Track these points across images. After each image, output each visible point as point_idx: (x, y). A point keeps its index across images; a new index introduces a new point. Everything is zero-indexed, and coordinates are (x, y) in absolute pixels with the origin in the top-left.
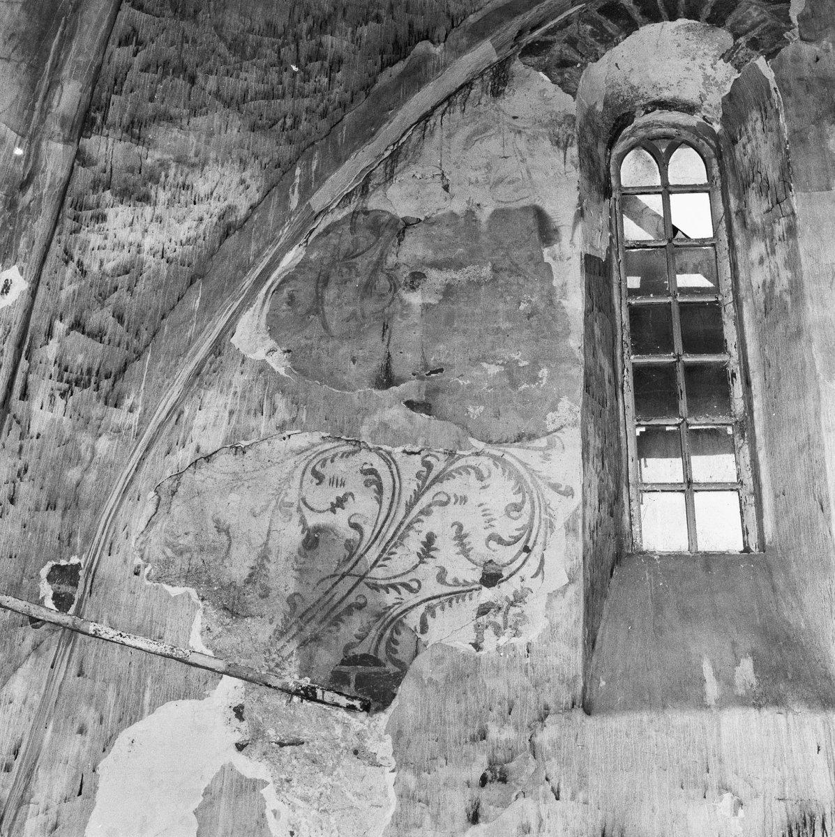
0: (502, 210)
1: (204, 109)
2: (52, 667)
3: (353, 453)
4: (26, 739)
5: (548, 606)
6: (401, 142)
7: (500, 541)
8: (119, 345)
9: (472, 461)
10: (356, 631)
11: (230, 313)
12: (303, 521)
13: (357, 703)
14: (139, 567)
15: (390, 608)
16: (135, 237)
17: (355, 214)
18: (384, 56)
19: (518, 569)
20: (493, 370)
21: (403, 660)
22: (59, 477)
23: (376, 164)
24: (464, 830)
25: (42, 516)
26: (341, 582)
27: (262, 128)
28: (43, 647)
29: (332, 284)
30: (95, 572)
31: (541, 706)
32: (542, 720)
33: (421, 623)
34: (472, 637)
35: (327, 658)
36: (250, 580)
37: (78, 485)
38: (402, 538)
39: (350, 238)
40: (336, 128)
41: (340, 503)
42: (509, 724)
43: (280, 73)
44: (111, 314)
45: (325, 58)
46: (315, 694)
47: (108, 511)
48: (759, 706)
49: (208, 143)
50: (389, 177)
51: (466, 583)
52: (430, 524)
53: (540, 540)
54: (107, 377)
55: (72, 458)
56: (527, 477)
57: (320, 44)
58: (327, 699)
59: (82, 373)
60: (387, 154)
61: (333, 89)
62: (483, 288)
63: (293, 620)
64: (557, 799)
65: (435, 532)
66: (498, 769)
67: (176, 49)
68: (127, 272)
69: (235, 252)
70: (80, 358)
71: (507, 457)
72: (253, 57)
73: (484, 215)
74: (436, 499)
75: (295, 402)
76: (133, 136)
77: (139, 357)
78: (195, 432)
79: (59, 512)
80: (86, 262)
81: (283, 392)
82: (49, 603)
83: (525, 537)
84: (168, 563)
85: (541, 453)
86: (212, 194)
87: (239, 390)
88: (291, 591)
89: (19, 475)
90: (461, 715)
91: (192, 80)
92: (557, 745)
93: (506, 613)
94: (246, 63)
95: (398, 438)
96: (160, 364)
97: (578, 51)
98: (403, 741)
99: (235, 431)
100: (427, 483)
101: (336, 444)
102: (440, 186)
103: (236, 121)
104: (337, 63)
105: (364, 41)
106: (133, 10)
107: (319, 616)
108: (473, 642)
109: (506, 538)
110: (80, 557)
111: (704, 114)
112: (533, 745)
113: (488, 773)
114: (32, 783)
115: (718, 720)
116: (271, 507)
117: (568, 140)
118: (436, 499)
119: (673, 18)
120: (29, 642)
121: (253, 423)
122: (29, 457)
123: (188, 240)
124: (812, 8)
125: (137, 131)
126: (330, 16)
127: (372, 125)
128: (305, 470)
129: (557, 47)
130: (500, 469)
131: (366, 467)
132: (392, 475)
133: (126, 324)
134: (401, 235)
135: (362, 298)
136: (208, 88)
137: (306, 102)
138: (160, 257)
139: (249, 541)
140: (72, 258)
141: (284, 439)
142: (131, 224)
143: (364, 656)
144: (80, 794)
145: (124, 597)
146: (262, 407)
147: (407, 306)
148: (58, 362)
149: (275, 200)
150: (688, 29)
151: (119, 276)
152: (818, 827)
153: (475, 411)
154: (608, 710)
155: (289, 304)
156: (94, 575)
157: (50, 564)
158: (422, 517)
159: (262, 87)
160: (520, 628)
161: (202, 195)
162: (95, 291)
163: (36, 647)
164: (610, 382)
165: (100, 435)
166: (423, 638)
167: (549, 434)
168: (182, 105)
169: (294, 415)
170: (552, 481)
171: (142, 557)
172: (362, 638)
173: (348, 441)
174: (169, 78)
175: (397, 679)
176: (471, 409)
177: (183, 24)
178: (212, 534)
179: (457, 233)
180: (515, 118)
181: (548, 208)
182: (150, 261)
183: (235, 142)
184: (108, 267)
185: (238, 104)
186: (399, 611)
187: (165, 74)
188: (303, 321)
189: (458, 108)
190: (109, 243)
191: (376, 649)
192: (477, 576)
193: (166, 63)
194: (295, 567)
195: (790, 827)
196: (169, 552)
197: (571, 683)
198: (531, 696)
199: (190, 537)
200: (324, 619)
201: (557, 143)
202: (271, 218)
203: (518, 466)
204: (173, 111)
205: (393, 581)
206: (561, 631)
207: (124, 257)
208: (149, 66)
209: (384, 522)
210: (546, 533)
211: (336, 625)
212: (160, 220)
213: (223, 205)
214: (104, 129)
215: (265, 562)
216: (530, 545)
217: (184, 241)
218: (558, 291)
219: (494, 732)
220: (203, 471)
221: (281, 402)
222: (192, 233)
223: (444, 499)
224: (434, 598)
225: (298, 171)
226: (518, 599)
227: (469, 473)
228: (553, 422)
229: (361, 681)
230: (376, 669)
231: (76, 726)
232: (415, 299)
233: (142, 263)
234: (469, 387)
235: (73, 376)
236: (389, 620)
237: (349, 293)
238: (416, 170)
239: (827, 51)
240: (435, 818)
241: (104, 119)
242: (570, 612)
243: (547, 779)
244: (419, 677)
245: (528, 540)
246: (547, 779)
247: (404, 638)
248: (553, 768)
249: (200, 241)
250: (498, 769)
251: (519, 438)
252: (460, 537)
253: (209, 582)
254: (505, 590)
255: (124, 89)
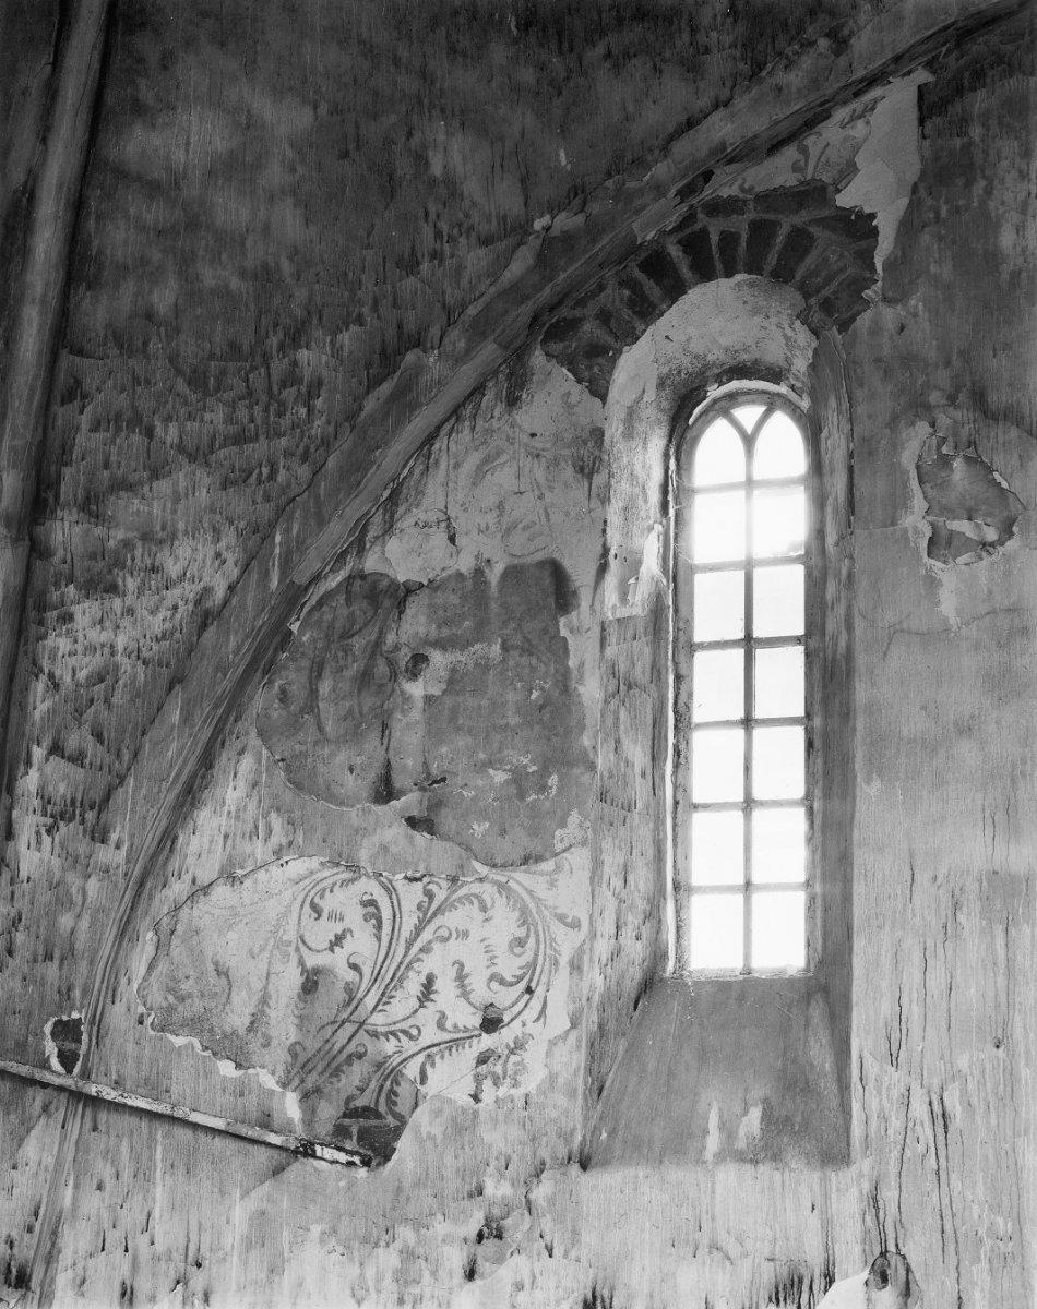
0: (515, 567)
1: (167, 468)
2: (63, 1128)
3: (353, 880)
4: (44, 1201)
5: (548, 1054)
6: (402, 476)
7: (502, 982)
8: (101, 770)
9: (476, 888)
10: (357, 1083)
11: (215, 720)
12: (301, 963)
13: (357, 1159)
14: (142, 1015)
15: (390, 1057)
16: (105, 636)
17: (350, 579)
18: (371, 371)
19: (520, 1013)
20: (500, 777)
21: (403, 1113)
22: (53, 925)
23: (374, 509)
24: (462, 1288)
25: (40, 968)
26: (341, 1029)
27: (234, 483)
28: (53, 1107)
29: (327, 672)
30: (100, 1022)
31: (537, 1162)
32: (538, 1175)
33: (421, 1073)
34: (471, 1088)
35: (328, 1112)
36: (252, 1028)
37: (72, 933)
38: (401, 981)
39: (344, 612)
40: (319, 476)
41: (338, 940)
42: (506, 1179)
43: (250, 407)
44: (90, 732)
45: (299, 381)
46: (314, 1151)
47: (104, 960)
48: (755, 1162)
49: (174, 512)
50: (389, 528)
51: (466, 1029)
52: (429, 964)
53: (544, 979)
54: (91, 809)
55: (62, 901)
56: (532, 906)
57: (295, 363)
58: (327, 1156)
59: (66, 805)
60: (386, 494)
61: (313, 422)
62: (491, 672)
63: (293, 1072)
64: (551, 1256)
65: (435, 973)
66: (494, 1225)
67: (127, 395)
68: (102, 680)
69: (214, 648)
70: (62, 788)
71: (511, 883)
72: (218, 389)
73: (494, 575)
74: (437, 934)
75: (291, 822)
76: (90, 514)
77: (121, 783)
78: (190, 860)
79: (56, 962)
80: (58, 673)
81: (278, 810)
82: (55, 1063)
83: (528, 977)
84: (171, 1009)
85: (548, 878)
86: (185, 574)
87: (233, 809)
88: (292, 1040)
89: (13, 925)
90: (458, 1171)
91: (149, 432)
92: (551, 1201)
93: (506, 1062)
94: (210, 401)
95: (398, 863)
96: (144, 791)
97: (611, 331)
98: (402, 1198)
99: (230, 858)
100: (429, 914)
101: (335, 870)
102: (445, 536)
103: (204, 478)
104: (317, 385)
105: (345, 354)
106: (71, 357)
107: (320, 1068)
108: (472, 1093)
109: (509, 979)
110: (80, 1013)
111: (793, 382)
112: (528, 1202)
113: (485, 1229)
114: (59, 1241)
115: (713, 1176)
116: (269, 948)
117: (594, 463)
118: (437, 934)
119: (729, 274)
120: (38, 1103)
121: (248, 848)
122: (22, 904)
123: (164, 635)
124: (903, 250)
125: (95, 508)
126: (303, 322)
127: (358, 470)
128: (303, 902)
129: (587, 327)
130: (505, 899)
131: (366, 898)
132: (393, 907)
133: (106, 743)
134: (401, 607)
135: (360, 691)
136: (169, 440)
137: (283, 442)
138: (135, 658)
139: (248, 984)
140: (42, 671)
141: (282, 865)
142: (101, 621)
143: (366, 1109)
144: (103, 1250)
145: (130, 1048)
146: (256, 828)
147: (407, 699)
148: (41, 794)
149: (255, 576)
150: (751, 285)
151: (94, 685)
152: (805, 1289)
153: (479, 828)
154: (605, 1163)
155: (281, 701)
156: (99, 1026)
157: (53, 1019)
158: (422, 956)
159: (232, 429)
160: (519, 1078)
161: (174, 578)
162: (70, 707)
163: (46, 1108)
164: (643, 775)
165: (89, 876)
166: (423, 1089)
167: (556, 855)
168: (141, 468)
169: (290, 838)
170: (559, 911)
171: (145, 1005)
172: (362, 1090)
173: (347, 867)
174: (123, 434)
175: (397, 1132)
176: (475, 827)
177: (131, 362)
178: (212, 977)
179: (464, 598)
180: (533, 435)
181: (567, 564)
182: (125, 664)
183: (206, 507)
184: (82, 675)
185: (205, 456)
186: (399, 1060)
187: (118, 430)
188: (294, 725)
189: (467, 423)
190: (79, 647)
191: (377, 1101)
192: (477, 1021)
193: (118, 416)
194: (296, 1013)
195: (777, 1288)
196: (171, 998)
197: (566, 1137)
198: (528, 1151)
199: (191, 981)
200: (325, 1070)
201: (582, 469)
202: (250, 603)
203: (526, 897)
204: (133, 478)
205: (393, 1028)
206: (561, 1080)
207: (97, 661)
208: (99, 423)
209: (384, 962)
210: (550, 971)
211: (337, 1076)
212: (130, 611)
213: (198, 587)
214: (59, 511)
215: (266, 1008)
216: (533, 985)
217: (160, 636)
218: (575, 673)
219: (489, 1190)
220: (201, 906)
221: (276, 821)
222: (168, 625)
223: (446, 934)
224: (434, 1046)
225: (278, 538)
226: (518, 1046)
227: (472, 903)
228: (562, 841)
229: (363, 1136)
230: (374, 1122)
231: (95, 1182)
232: (416, 689)
233: (117, 667)
234: (473, 799)
235: (57, 809)
236: (388, 1071)
237: (345, 686)
238: (419, 514)
239: (915, 315)
240: (434, 1273)
241: (57, 497)
242: (571, 1060)
243: (541, 1236)
244: (417, 1133)
245: (531, 980)
246: (541, 1236)
247: (404, 1090)
248: (547, 1224)
249: (177, 635)
250: (494, 1225)
251: (525, 861)
252: (461, 978)
253: (211, 1030)
254: (506, 1035)
255: (74, 457)
